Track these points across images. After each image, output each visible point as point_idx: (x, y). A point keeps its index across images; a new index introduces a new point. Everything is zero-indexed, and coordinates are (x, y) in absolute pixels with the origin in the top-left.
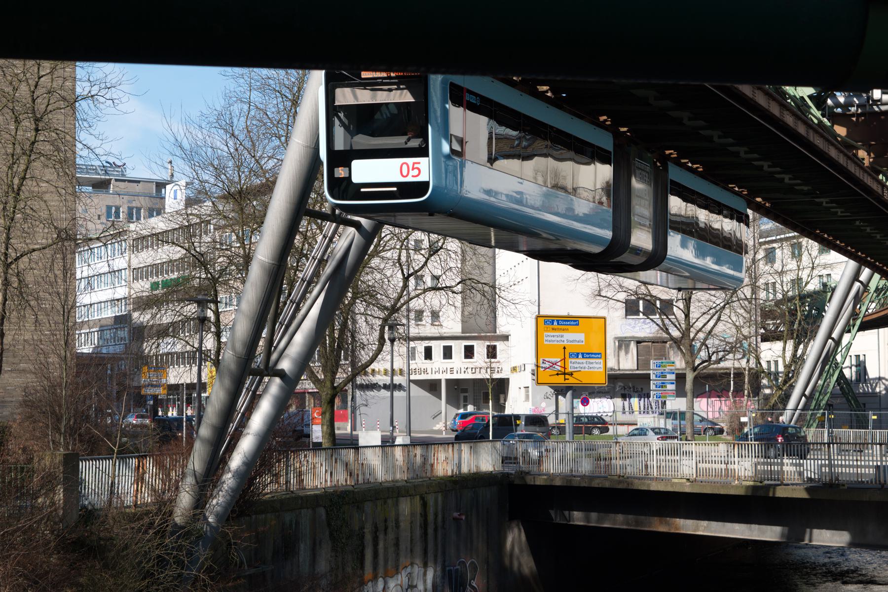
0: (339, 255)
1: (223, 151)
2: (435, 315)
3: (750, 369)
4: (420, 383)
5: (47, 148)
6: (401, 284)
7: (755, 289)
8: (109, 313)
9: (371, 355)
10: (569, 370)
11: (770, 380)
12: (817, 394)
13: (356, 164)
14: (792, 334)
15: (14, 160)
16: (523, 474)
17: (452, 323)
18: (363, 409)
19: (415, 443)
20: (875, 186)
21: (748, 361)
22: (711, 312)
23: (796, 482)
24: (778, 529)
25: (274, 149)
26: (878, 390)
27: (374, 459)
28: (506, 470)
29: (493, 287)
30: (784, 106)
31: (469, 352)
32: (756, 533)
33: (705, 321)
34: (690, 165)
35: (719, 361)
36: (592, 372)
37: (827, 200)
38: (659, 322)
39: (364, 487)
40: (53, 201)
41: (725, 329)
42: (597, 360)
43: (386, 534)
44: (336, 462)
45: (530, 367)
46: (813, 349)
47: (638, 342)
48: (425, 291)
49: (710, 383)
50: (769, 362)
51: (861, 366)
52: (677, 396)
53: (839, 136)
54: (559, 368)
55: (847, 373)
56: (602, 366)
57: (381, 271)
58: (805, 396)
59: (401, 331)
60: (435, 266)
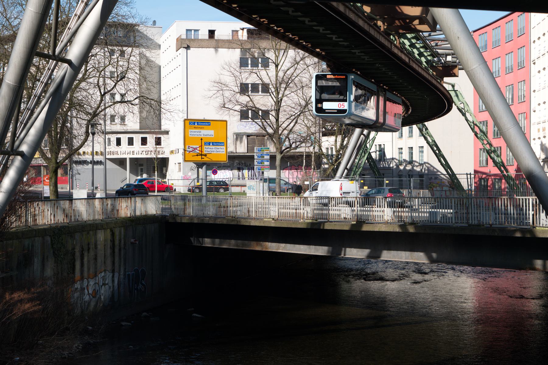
0: (58, 80)
2: (123, 119)
3: (315, 153)
4: (112, 160)
6: (99, 99)
9: (80, 142)
10: (204, 153)
11: (328, 160)
12: (355, 168)
13: (324, 103)
14: (341, 131)
16: (174, 216)
18: (77, 176)
20: (386, 43)
21: (314, 148)
22: (292, 118)
23: (337, 220)
24: (325, 249)
25: (18, 12)
26: (391, 165)
27: (81, 207)
28: (164, 213)
29: (159, 102)
31: (144, 141)
32: (313, 250)
33: (288, 123)
34: (275, 28)
35: (297, 147)
36: (218, 154)
37: (359, 51)
38: (260, 124)
39: (75, 223)
42: (222, 147)
43: (88, 252)
44: (57, 208)
45: (181, 151)
47: (248, 136)
48: (115, 103)
50: (327, 149)
51: (382, 151)
52: (271, 169)
53: (366, 12)
54: (198, 152)
55: (373, 155)
56: (224, 150)
57: (86, 90)
58: (347, 169)
59: (99, 128)
60: (120, 88)
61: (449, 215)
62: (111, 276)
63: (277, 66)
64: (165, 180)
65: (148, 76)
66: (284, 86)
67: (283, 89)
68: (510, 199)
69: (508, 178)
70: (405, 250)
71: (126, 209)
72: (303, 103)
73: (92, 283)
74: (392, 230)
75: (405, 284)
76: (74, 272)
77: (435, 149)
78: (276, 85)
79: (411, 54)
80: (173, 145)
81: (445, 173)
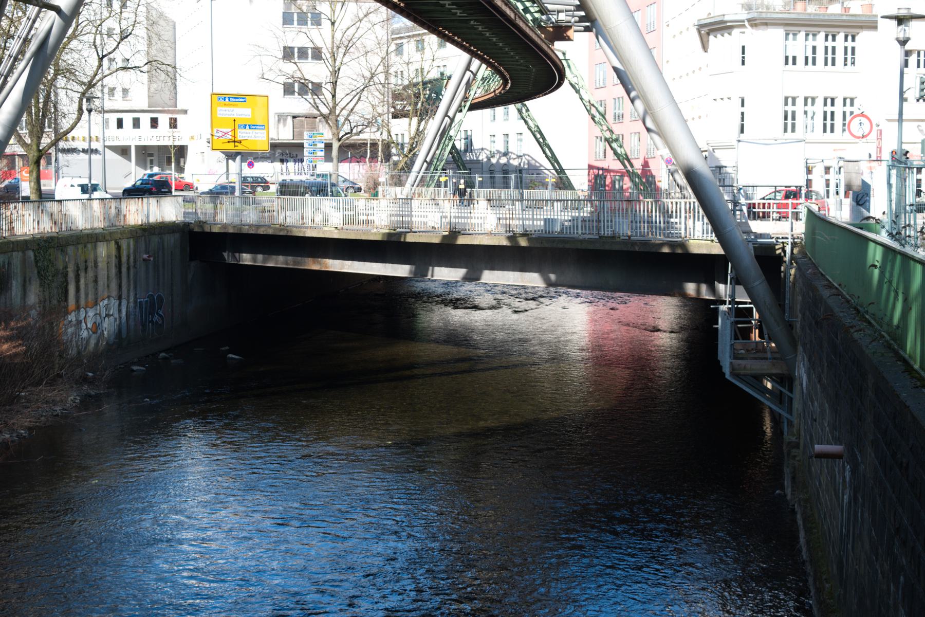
0: (41, 35)
3: (383, 140)
6: (96, 63)
10: (238, 139)
16: (201, 224)
28: (187, 220)
36: (258, 140)
38: (312, 102)
39: (67, 233)
43: (86, 272)
47: (294, 117)
52: (326, 161)
60: (125, 50)
61: (566, 224)
62: (117, 303)
63: (333, 24)
64: (182, 175)
65: (162, 33)
66: (342, 50)
67: (341, 55)
68: (656, 202)
70: (513, 270)
71: (137, 213)
72: (368, 75)
73: (91, 313)
74: (497, 244)
76: (66, 300)
77: (538, 136)
78: (332, 48)
80: (193, 132)
81: (550, 167)
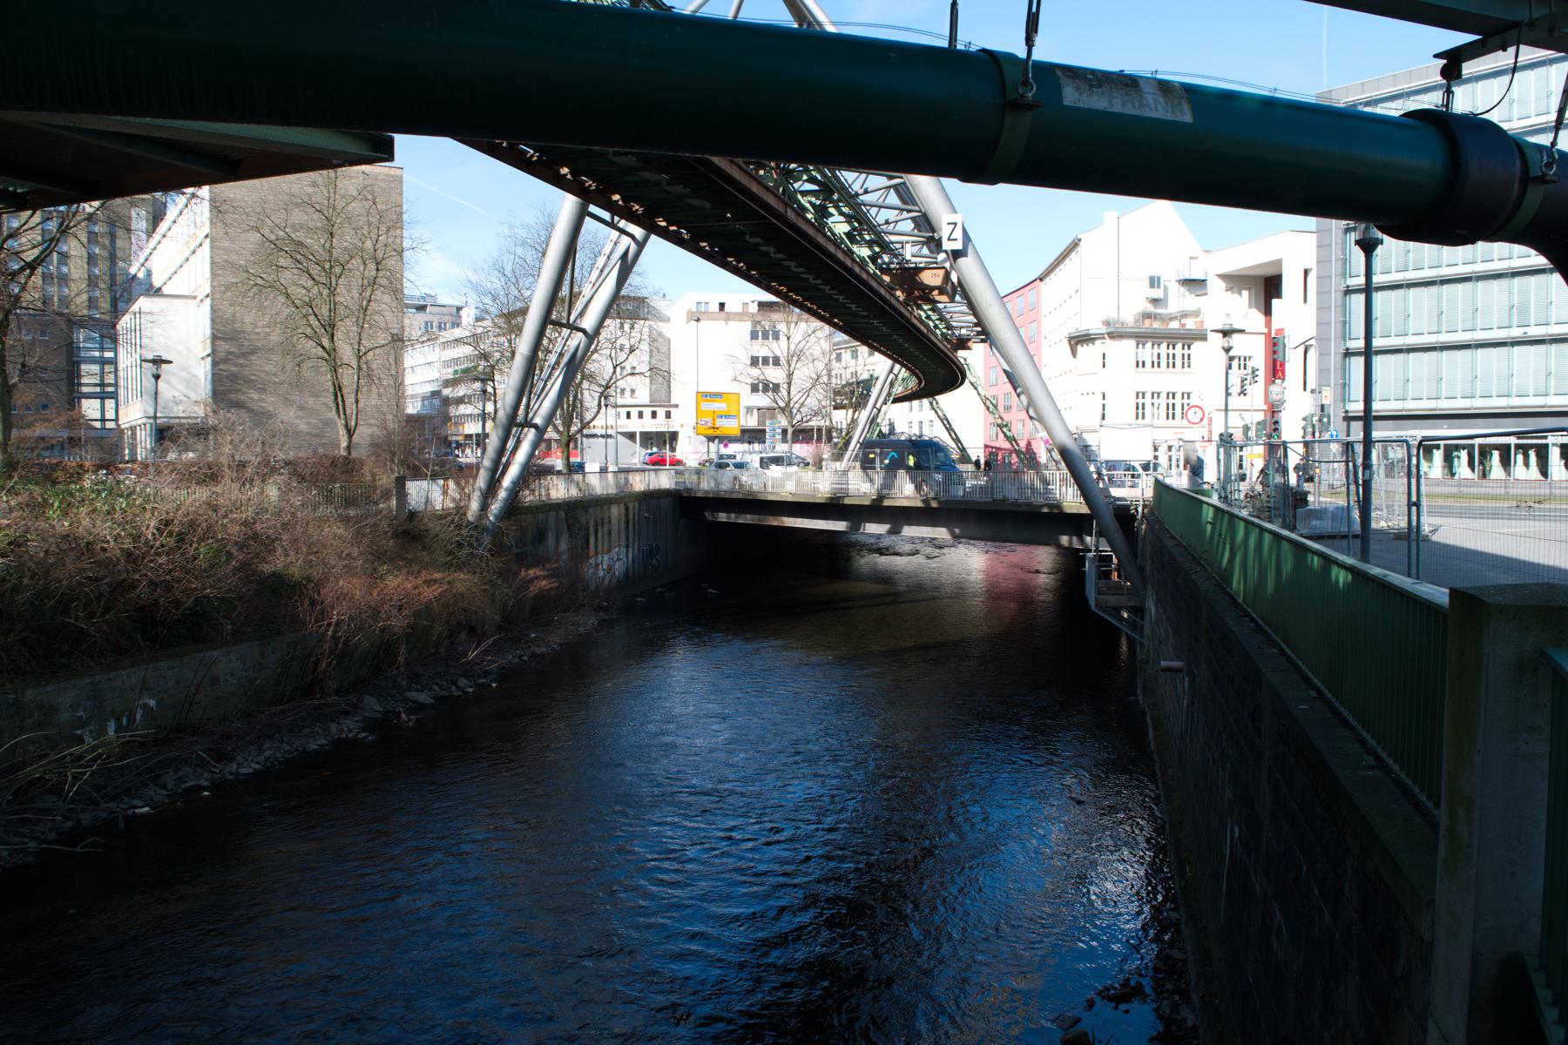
1: (498, 285)
2: (633, 391)
4: (623, 434)
5: (385, 282)
7: (830, 376)
8: (428, 389)
15: (363, 288)
16: (688, 490)
17: (643, 396)
19: (621, 471)
30: (853, 260)
31: (654, 415)
33: (1497, 266)
36: (731, 427)
40: (388, 316)
41: (812, 402)
46: (864, 415)
49: (802, 434)
51: (892, 426)
69: (1018, 453)
75: (919, 560)
79: (927, 326)
80: (683, 421)
